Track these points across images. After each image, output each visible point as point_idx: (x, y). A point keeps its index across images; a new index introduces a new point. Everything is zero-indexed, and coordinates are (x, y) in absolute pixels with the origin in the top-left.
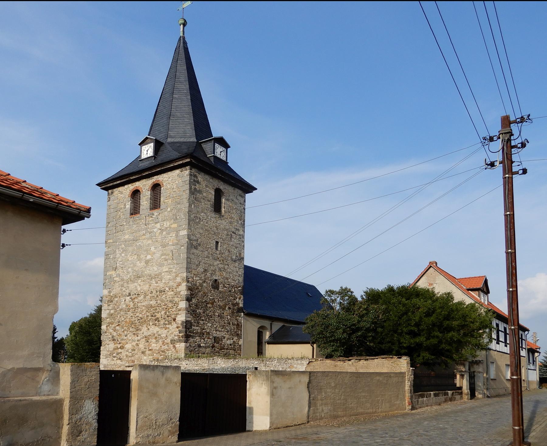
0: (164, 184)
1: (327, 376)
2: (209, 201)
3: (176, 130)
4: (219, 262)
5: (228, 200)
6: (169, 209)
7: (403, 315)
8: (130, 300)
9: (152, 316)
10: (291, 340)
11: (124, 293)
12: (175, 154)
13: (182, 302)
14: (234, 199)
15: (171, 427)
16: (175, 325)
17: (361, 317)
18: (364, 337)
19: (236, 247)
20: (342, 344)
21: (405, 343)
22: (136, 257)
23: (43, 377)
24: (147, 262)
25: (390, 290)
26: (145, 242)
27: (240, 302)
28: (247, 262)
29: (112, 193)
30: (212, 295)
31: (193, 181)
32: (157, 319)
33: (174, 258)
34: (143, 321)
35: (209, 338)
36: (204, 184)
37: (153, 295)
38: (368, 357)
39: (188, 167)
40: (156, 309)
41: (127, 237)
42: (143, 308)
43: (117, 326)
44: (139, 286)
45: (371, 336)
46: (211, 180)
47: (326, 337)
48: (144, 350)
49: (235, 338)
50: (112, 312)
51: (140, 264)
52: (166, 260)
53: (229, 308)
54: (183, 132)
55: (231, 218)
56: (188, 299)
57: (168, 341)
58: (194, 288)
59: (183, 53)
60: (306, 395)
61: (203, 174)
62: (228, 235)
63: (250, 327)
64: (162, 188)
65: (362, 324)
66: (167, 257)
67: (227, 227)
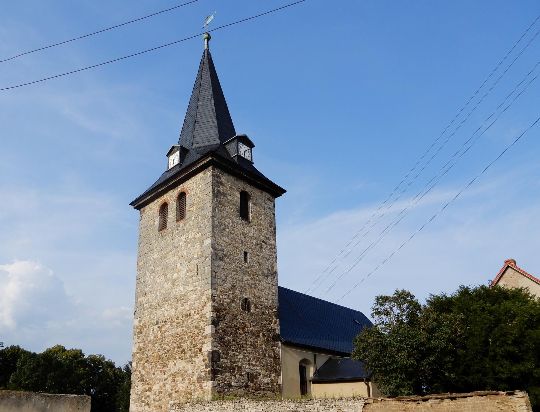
0: (189, 191)
3: (201, 135)
4: (249, 277)
5: (255, 204)
6: (193, 218)
7: (491, 329)
8: (158, 329)
9: (178, 347)
11: (153, 321)
13: (208, 326)
14: (262, 204)
16: (201, 358)
17: (432, 331)
19: (268, 259)
20: (410, 375)
21: (503, 373)
22: (163, 277)
24: (174, 282)
25: (465, 292)
26: (171, 258)
27: (276, 327)
28: (283, 282)
29: (144, 211)
30: (243, 318)
31: (216, 183)
32: (183, 352)
33: (199, 273)
34: (169, 355)
35: (241, 375)
36: (228, 186)
37: (179, 321)
38: (455, 395)
39: (210, 168)
40: (182, 339)
41: (156, 256)
42: (170, 338)
43: (146, 362)
44: (166, 312)
46: (236, 182)
47: (385, 366)
48: (171, 392)
49: (273, 375)
50: (142, 345)
51: (168, 285)
52: (191, 277)
54: (208, 135)
55: (260, 225)
56: (215, 323)
57: (195, 379)
58: (221, 308)
59: (208, 63)
61: (227, 175)
62: (257, 244)
63: (290, 359)
64: (187, 196)
66: (192, 273)
67: (256, 235)
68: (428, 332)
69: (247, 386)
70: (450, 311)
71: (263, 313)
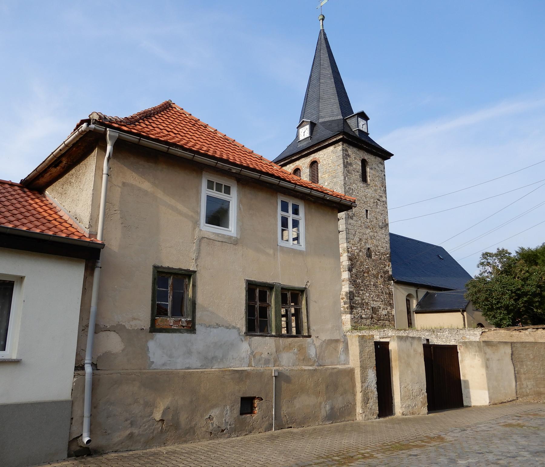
0: (321, 161)
1: (525, 347)
2: (358, 172)
10: (431, 309)
12: (327, 133)
14: (376, 167)
15: (422, 398)
17: (525, 280)
18: (530, 303)
23: (340, 348)
28: (393, 229)
31: (346, 156)
35: (368, 309)
39: (340, 143)
45: (538, 301)
49: (389, 308)
53: (381, 276)
54: (331, 112)
56: (350, 270)
60: (511, 367)
62: (374, 203)
63: (400, 294)
64: (319, 165)
65: (527, 288)
67: (373, 195)
68: (522, 280)
69: (372, 318)
70: (536, 264)
71: (380, 259)
